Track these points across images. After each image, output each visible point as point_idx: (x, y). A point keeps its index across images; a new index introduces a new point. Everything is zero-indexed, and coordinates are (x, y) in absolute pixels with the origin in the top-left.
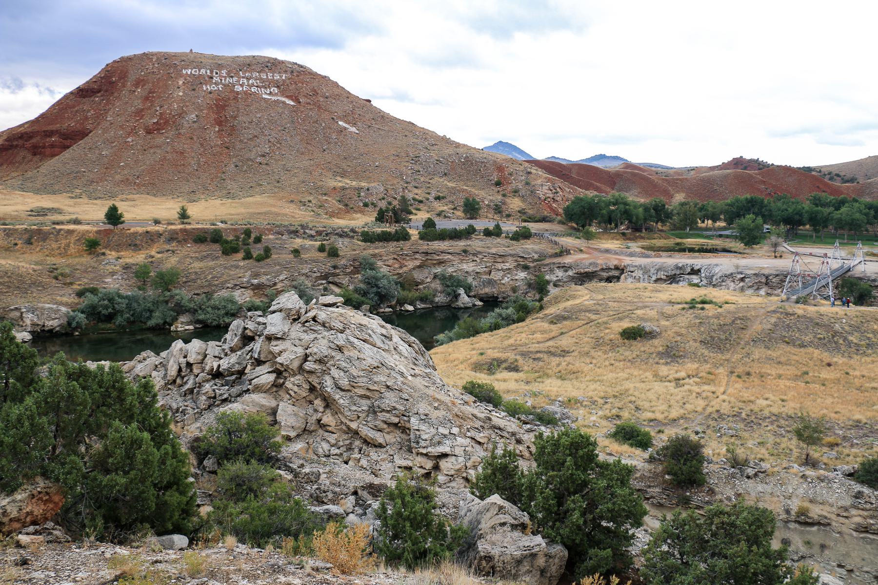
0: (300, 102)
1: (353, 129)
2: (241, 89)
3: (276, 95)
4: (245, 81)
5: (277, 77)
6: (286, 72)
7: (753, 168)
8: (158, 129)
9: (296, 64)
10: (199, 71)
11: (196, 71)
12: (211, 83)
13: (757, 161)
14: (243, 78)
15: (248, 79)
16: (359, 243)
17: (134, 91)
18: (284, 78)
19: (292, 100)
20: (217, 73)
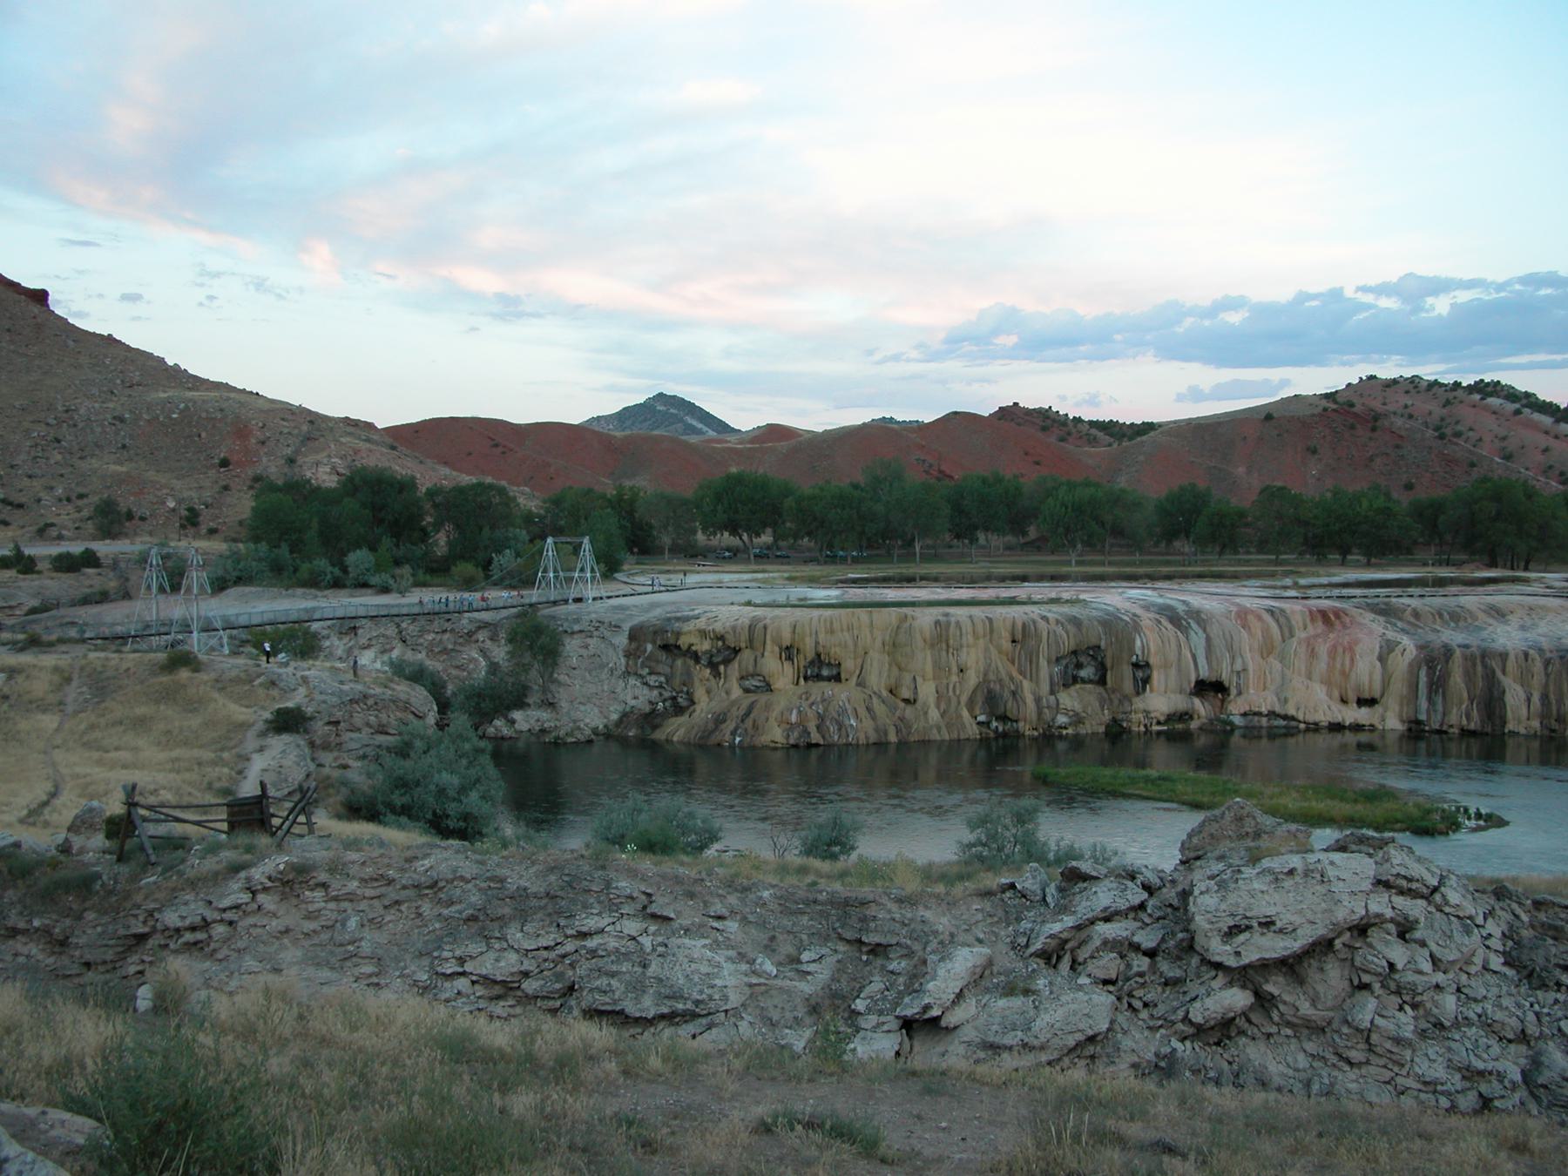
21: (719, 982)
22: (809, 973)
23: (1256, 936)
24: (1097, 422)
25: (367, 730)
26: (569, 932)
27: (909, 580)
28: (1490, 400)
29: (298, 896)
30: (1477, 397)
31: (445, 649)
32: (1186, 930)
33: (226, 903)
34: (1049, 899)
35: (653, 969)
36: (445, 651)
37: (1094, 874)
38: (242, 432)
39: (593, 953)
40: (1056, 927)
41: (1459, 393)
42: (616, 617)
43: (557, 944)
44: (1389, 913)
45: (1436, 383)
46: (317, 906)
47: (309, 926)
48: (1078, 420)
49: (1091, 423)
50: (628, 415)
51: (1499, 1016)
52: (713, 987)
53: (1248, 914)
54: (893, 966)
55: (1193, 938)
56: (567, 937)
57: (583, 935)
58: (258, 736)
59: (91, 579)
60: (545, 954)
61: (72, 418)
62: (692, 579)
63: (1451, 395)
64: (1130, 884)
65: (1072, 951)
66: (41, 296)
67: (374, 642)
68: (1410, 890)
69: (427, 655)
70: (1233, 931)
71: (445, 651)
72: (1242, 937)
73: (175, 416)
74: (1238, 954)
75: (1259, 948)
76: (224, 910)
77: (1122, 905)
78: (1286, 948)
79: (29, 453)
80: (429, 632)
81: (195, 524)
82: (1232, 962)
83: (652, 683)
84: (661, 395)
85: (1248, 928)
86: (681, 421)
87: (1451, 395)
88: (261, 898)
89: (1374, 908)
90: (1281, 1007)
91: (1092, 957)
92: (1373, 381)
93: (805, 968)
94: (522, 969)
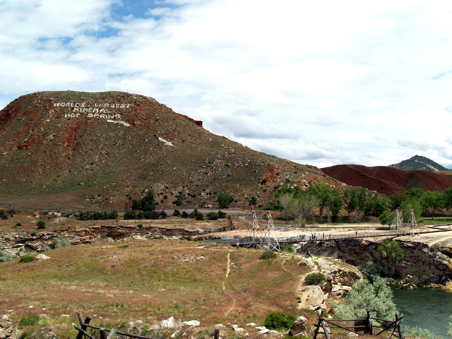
0: (134, 125)
1: (170, 144)
2: (92, 116)
3: (119, 119)
4: (97, 110)
5: (123, 106)
6: (130, 103)
7: (421, 160)
8: (26, 146)
9: (142, 96)
10: (66, 104)
11: (63, 105)
12: (72, 112)
13: (403, 162)
14: (97, 108)
15: (100, 109)
16: (123, 221)
17: (20, 120)
18: (128, 107)
19: (129, 123)
20: (78, 105)
25: (339, 284)
31: (356, 252)
36: (356, 253)
38: (271, 169)
42: (426, 241)
50: (404, 163)
59: (222, 222)
61: (211, 166)
66: (200, 123)
67: (328, 249)
69: (349, 255)
71: (356, 253)
73: (246, 164)
79: (197, 177)
81: (254, 204)
83: (440, 268)
84: (416, 156)
86: (425, 166)
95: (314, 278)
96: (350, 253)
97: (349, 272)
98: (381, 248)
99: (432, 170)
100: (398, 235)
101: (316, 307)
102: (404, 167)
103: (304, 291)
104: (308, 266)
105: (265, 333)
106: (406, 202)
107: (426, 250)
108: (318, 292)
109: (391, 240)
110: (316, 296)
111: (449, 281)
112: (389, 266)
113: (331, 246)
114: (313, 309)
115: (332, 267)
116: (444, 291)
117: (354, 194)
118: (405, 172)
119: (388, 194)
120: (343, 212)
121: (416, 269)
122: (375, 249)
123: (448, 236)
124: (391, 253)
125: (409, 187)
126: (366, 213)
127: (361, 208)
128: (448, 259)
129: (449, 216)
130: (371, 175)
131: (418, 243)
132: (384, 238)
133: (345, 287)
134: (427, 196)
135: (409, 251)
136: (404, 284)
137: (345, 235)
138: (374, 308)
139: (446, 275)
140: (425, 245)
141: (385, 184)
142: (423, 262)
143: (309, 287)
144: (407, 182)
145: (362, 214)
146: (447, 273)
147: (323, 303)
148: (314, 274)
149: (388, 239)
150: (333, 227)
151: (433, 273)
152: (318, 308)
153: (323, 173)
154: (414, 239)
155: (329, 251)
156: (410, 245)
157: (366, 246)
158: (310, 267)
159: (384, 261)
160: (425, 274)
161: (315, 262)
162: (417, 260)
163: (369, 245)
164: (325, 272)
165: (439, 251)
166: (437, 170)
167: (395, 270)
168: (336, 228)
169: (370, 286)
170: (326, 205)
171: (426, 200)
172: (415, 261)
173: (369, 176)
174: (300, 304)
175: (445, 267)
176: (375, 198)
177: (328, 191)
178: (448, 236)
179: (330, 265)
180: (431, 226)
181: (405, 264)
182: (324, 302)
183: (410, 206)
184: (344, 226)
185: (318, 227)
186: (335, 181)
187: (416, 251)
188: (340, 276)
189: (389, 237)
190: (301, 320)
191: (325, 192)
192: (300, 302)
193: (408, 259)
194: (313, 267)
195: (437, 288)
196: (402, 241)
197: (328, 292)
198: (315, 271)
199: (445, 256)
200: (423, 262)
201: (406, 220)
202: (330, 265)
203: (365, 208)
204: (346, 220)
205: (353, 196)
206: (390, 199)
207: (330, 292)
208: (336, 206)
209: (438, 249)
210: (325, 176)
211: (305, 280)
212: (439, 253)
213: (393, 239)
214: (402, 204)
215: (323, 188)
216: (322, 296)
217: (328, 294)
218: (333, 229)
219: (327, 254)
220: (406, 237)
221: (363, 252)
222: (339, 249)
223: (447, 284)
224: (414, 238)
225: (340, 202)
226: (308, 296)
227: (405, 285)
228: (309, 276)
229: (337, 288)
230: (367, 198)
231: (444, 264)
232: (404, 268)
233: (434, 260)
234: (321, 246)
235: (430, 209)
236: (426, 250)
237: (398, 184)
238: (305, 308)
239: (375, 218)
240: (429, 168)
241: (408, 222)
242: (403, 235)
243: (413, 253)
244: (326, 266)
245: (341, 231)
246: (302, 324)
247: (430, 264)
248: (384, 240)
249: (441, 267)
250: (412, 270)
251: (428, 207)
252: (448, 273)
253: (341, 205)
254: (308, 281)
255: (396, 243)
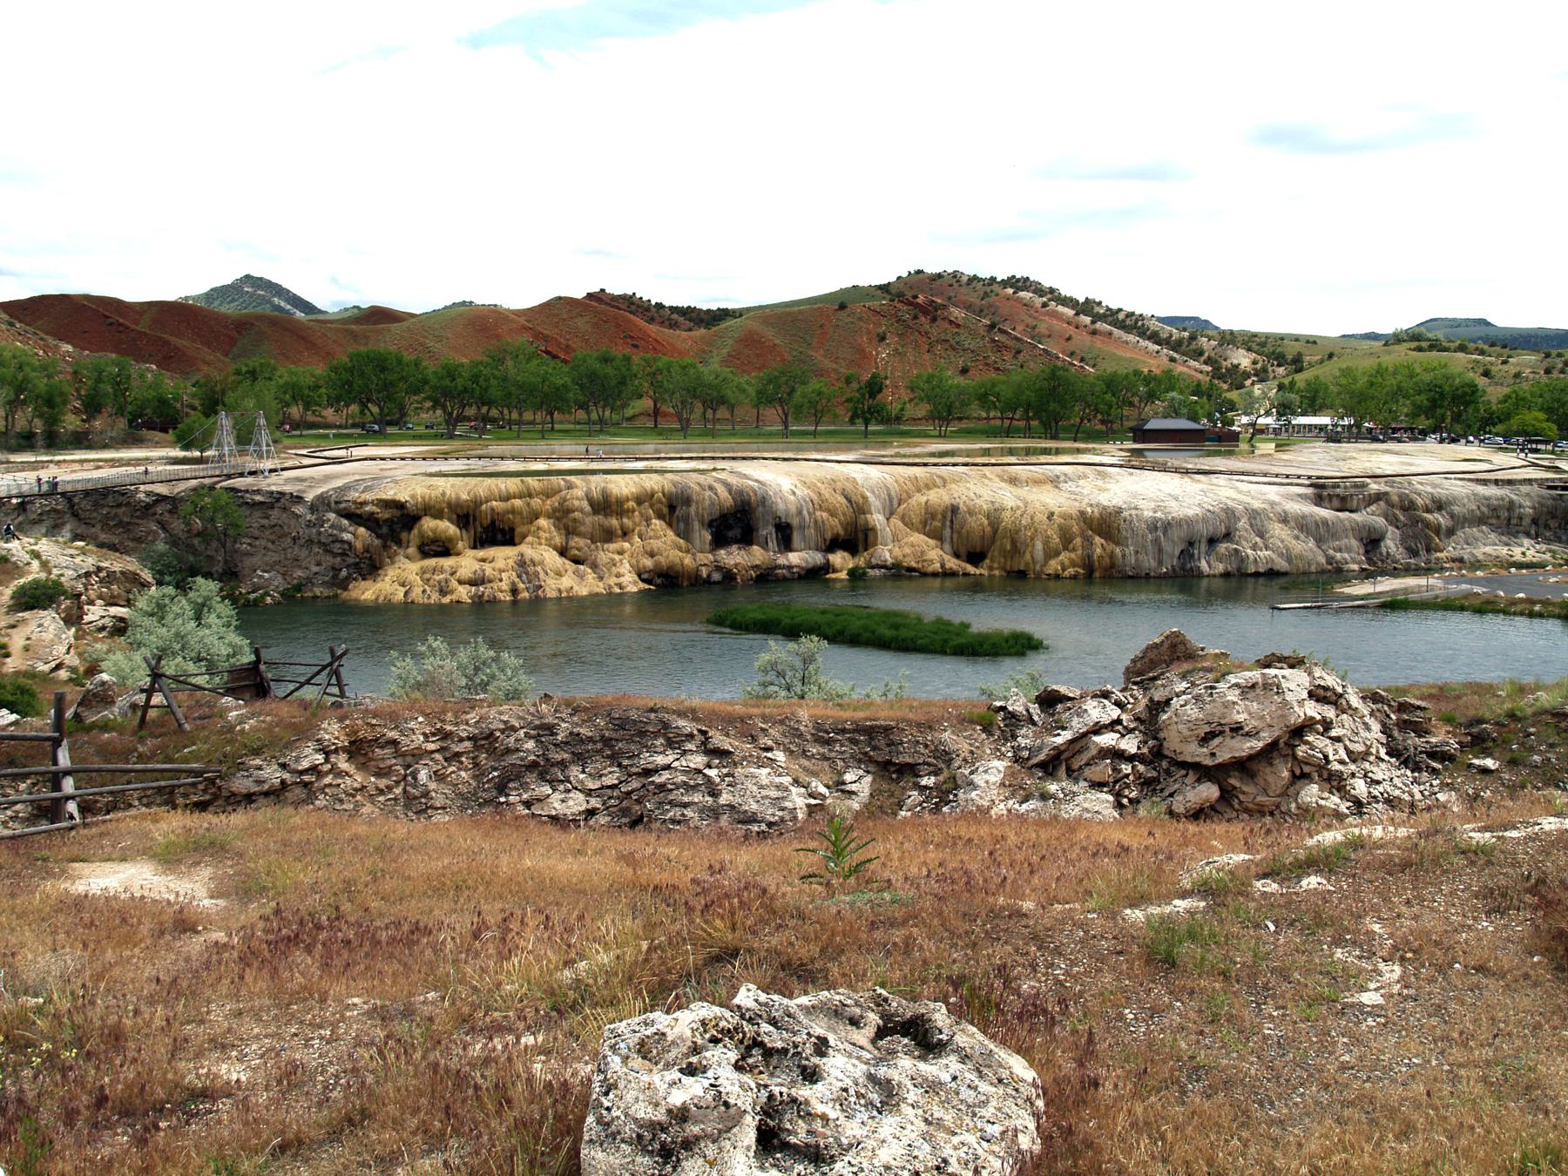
21: (788, 804)
22: (853, 793)
23: (1228, 739)
24: (677, 308)
26: (634, 770)
27: (1078, 451)
28: (1022, 294)
29: (366, 754)
30: (1010, 291)
31: (121, 522)
32: (1155, 738)
33: (305, 764)
34: (1036, 718)
35: (725, 798)
36: (121, 524)
37: (1071, 695)
39: (662, 787)
40: (1059, 740)
41: (995, 287)
42: (298, 488)
43: (621, 782)
44: (1318, 717)
45: (975, 278)
46: (389, 763)
47: (382, 783)
48: (660, 306)
49: (671, 308)
51: (1397, 793)
52: (783, 809)
53: (1223, 722)
54: (925, 781)
55: (1161, 745)
56: (630, 776)
57: (648, 772)
58: (7, 613)
60: (609, 792)
62: (358, 452)
63: (988, 289)
64: (1106, 702)
65: (1066, 760)
68: (1325, 697)
69: (102, 529)
70: (1206, 739)
71: (121, 524)
72: (1216, 741)
74: (1213, 755)
75: (1231, 750)
76: (302, 773)
77: (1106, 720)
78: (1252, 748)
80: (103, 506)
82: (1208, 762)
84: (248, 277)
85: (1221, 732)
86: (270, 302)
87: (988, 289)
88: (333, 759)
89: (1311, 713)
90: (1242, 797)
91: (1088, 764)
92: (921, 276)
93: (848, 787)
94: (589, 807)
95: (38, 592)
96: (106, 526)
97: (122, 573)
98: (188, 507)
99: (288, 312)
100: (229, 477)
101: (53, 664)
102: (216, 303)
103: (14, 627)
104: (15, 563)
105: (11, 724)
106: (239, 392)
107: (299, 509)
108: (53, 627)
109: (212, 488)
110: (48, 636)
111: (355, 579)
112: (209, 553)
113: (55, 510)
114: (46, 668)
115: (78, 560)
116: (345, 602)
117: (100, 373)
118: (225, 317)
119: (185, 374)
120: (71, 422)
121: (276, 557)
122: (170, 512)
123: (348, 474)
124: (212, 520)
125: (239, 356)
126: (130, 422)
127: (121, 411)
128: (351, 529)
129: (340, 427)
130: (136, 322)
131: (278, 493)
132: (194, 483)
133: (114, 610)
134: (286, 378)
135: (257, 514)
136: (249, 593)
137: (89, 480)
138: (199, 653)
139: (348, 567)
140: (297, 497)
141: (176, 348)
142: (294, 539)
143: (26, 614)
144: (232, 342)
145: (122, 423)
146: (351, 560)
147: (68, 653)
148: (36, 582)
149: (203, 486)
150: (51, 462)
151: (319, 564)
152: (58, 667)
153: (5, 317)
154: (269, 485)
155: (49, 523)
156: (258, 498)
157: (148, 506)
158: (21, 564)
159: (196, 541)
160: (300, 567)
161: (33, 552)
162: (278, 531)
163: (156, 502)
164: (62, 575)
165: (331, 510)
166: (299, 315)
167: (226, 562)
168: (59, 462)
169: (180, 601)
170: (24, 402)
171: (285, 388)
172: (273, 537)
173: (133, 327)
174: (8, 660)
175: (346, 546)
176: (156, 385)
177: (28, 364)
178: (348, 474)
179: (72, 556)
180: (304, 452)
181: (250, 544)
182: (72, 650)
183: (250, 403)
184: (83, 457)
185: (8, 462)
186: (42, 339)
187: (275, 513)
188: (101, 582)
189: (207, 481)
190: (103, 683)
191: (20, 367)
192: (8, 655)
193: (257, 533)
194: (29, 564)
195: (328, 597)
196: (241, 491)
197: (73, 625)
198: (35, 572)
199: (345, 522)
200: (294, 539)
201: (245, 438)
202: (72, 556)
203: (130, 408)
204: (81, 441)
205: (99, 380)
206: (194, 386)
207: (80, 624)
208: (50, 404)
209: (329, 505)
210: (12, 325)
211: (12, 598)
212: (332, 516)
213: (218, 486)
214: (230, 398)
215: (14, 357)
216: (64, 636)
217: (73, 630)
218: (51, 465)
219: (44, 530)
220: (250, 480)
221: (140, 521)
222: (75, 515)
223: (351, 586)
224: (268, 481)
225: (62, 394)
226: (28, 639)
227: (252, 596)
228: (23, 587)
229: (95, 613)
230: (134, 384)
231: (343, 542)
232: (248, 554)
233: (319, 533)
234: (25, 510)
235: (295, 411)
236: (299, 509)
237: (209, 348)
238: (24, 668)
239: (159, 436)
240: (278, 308)
241: (241, 447)
242: (241, 475)
243: (267, 517)
244: (64, 561)
245: (75, 471)
246: (104, 691)
247: (310, 541)
248: (195, 489)
249: (337, 548)
250: (267, 559)
251: (288, 405)
252: (352, 561)
253: (65, 402)
254: (23, 600)
255: (225, 497)
